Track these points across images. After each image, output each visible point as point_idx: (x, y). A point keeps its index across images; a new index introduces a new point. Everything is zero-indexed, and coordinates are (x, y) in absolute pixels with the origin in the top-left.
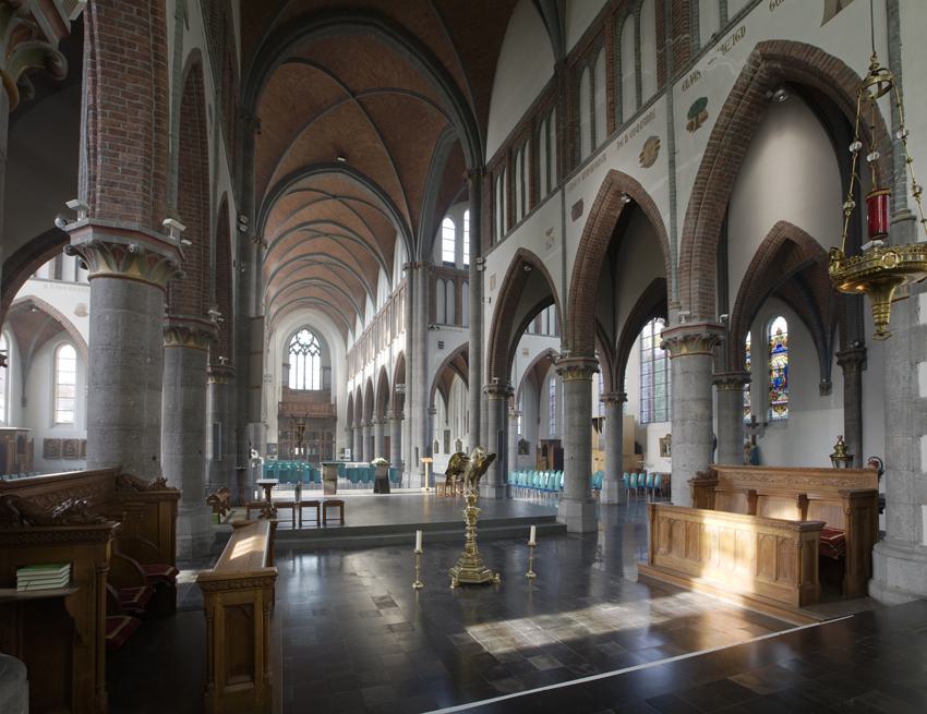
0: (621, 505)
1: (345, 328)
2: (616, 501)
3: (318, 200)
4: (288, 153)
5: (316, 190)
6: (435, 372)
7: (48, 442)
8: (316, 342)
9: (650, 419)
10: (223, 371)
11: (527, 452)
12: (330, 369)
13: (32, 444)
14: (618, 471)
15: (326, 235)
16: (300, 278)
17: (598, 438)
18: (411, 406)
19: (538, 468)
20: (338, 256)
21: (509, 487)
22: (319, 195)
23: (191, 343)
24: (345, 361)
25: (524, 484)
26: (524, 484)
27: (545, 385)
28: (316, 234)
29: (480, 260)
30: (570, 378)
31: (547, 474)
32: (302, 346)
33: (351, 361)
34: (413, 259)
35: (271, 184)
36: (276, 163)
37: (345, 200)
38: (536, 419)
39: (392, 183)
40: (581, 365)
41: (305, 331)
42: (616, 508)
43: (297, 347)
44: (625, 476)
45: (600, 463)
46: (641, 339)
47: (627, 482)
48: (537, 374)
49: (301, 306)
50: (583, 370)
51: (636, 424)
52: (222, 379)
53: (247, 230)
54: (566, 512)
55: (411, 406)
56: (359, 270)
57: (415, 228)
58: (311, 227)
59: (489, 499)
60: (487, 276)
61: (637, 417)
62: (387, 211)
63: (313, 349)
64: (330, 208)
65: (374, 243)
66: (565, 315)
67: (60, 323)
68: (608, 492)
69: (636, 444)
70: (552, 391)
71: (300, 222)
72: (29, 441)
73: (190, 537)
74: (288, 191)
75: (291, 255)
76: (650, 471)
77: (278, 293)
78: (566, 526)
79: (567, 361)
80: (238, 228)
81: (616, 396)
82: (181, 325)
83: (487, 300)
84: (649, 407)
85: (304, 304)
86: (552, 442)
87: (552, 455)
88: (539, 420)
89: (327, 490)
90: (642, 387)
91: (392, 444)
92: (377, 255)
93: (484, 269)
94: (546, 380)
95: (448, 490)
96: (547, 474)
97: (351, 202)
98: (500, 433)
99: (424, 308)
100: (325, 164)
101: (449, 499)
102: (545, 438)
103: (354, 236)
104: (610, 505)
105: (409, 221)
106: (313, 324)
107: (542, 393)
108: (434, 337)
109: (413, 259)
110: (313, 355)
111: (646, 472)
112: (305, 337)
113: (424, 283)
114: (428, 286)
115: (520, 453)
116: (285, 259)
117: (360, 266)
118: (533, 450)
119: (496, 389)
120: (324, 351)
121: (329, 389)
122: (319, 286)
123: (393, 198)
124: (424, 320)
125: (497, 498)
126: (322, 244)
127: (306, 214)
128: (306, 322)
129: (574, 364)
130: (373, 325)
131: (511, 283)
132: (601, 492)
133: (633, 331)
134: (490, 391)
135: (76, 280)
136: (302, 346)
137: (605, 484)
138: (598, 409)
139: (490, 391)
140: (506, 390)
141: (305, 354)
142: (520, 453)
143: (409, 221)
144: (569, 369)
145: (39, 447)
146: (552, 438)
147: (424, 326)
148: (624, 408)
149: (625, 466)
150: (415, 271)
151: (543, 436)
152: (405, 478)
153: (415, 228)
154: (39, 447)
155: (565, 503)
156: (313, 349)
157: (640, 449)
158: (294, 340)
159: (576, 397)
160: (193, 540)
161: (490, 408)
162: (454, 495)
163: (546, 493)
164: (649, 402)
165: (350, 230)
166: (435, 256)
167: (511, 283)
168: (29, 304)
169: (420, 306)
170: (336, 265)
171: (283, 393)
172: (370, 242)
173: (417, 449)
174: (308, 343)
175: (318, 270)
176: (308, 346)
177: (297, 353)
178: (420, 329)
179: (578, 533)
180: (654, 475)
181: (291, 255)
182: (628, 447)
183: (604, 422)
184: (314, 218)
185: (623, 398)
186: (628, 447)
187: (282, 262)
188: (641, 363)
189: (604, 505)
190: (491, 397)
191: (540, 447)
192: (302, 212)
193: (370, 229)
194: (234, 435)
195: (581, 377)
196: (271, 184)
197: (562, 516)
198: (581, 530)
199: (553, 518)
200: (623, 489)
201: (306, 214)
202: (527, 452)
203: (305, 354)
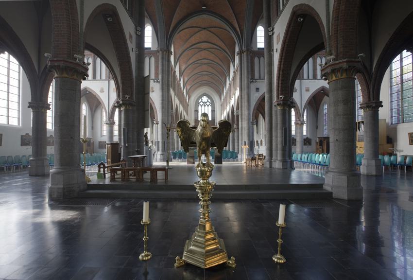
0: (378, 176)
1: (220, 94)
3: (199, 31)
5: (196, 27)
6: (255, 104)
7: (100, 142)
8: (209, 100)
9: (399, 121)
10: (128, 102)
12: (214, 111)
13: (93, 143)
15: (205, 49)
16: (196, 72)
17: (362, 132)
18: (242, 121)
19: (317, 152)
21: (292, 162)
22: (197, 29)
23: (65, 75)
24: (220, 107)
26: (306, 160)
28: (200, 50)
30: (334, 78)
32: (204, 103)
33: (223, 107)
37: (209, 29)
38: (315, 123)
39: (229, 13)
41: (205, 97)
43: (201, 103)
44: (380, 157)
45: (362, 148)
46: (391, 71)
48: (315, 102)
50: (346, 70)
52: (128, 107)
53: (141, 34)
54: (334, 183)
55: (242, 121)
56: (220, 63)
57: (242, 34)
59: (278, 169)
60: (275, 37)
61: (388, 120)
62: (228, 28)
63: (208, 103)
64: (203, 35)
66: (329, 31)
67: (95, 96)
70: (325, 111)
71: (191, 45)
72: (92, 142)
73: (62, 186)
75: (191, 61)
76: (399, 154)
78: (331, 193)
81: (373, 103)
82: (56, 64)
83: (275, 50)
84: (398, 113)
85: (201, 85)
87: (323, 145)
90: (391, 102)
92: (227, 53)
93: (273, 34)
95: (253, 163)
97: (212, 29)
99: (248, 72)
101: (254, 168)
102: (321, 136)
103: (216, 47)
104: (368, 176)
106: (207, 93)
108: (253, 86)
109: (241, 49)
110: (208, 106)
112: (205, 99)
113: (247, 59)
114: (250, 61)
115: (305, 144)
116: (189, 63)
118: (313, 143)
120: (213, 104)
121: (214, 120)
122: (207, 75)
123: (231, 21)
125: (283, 168)
127: (193, 40)
128: (203, 93)
129: (337, 67)
130: (229, 88)
133: (385, 63)
134: (278, 105)
135: (101, 78)
136: (204, 103)
137: (364, 162)
138: (360, 114)
139: (278, 105)
140: (289, 103)
141: (205, 106)
142: (305, 144)
144: (333, 71)
145: (97, 145)
146: (325, 136)
147: (248, 81)
148: (380, 113)
149: (381, 151)
150: (242, 55)
151: (319, 136)
152: (239, 156)
153: (242, 34)
154: (97, 145)
155: (330, 175)
156: (208, 103)
157: (391, 140)
158: (200, 101)
159: (340, 92)
160: (63, 188)
161: (278, 117)
163: (320, 166)
164: (398, 110)
165: (214, 44)
166: (253, 45)
168: (86, 89)
169: (245, 71)
170: (212, 64)
171: (195, 122)
172: (222, 47)
173: (245, 142)
174: (206, 101)
176: (206, 103)
177: (201, 106)
178: (246, 82)
179: (343, 200)
181: (191, 61)
182: (382, 139)
183: (362, 126)
186: (382, 139)
187: (187, 65)
188: (391, 94)
189: (364, 175)
190: (279, 108)
191: (318, 141)
192: (191, 39)
193: (223, 41)
194: (136, 134)
195: (344, 76)
196: (172, 25)
198: (346, 198)
199: (320, 186)
200: (379, 164)
201: (193, 40)
203: (205, 106)
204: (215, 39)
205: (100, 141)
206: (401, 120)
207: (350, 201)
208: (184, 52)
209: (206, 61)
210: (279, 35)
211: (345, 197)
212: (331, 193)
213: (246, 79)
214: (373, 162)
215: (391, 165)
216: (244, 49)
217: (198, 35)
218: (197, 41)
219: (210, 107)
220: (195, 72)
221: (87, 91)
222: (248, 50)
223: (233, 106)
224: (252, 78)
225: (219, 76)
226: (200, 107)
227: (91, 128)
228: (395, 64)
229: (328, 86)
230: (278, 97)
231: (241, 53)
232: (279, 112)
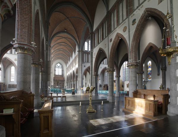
0: (119, 97)
1: (66, 63)
4: (55, 29)
7: (9, 85)
8: (61, 66)
11: (101, 87)
12: (63, 71)
14: (119, 91)
20: (65, 49)
22: (61, 37)
23: (37, 66)
27: (105, 74)
29: (92, 50)
35: (52, 35)
38: (103, 80)
39: (75, 35)
40: (112, 70)
41: (59, 64)
42: (118, 98)
43: (57, 67)
45: (115, 89)
49: (57, 59)
54: (109, 98)
60: (94, 53)
61: (122, 80)
63: (60, 67)
65: (72, 47)
69: (122, 85)
70: (106, 75)
72: (6, 84)
75: (56, 49)
76: (125, 90)
78: (109, 101)
81: (118, 76)
88: (103, 81)
89: (63, 94)
97: (68, 39)
104: (117, 97)
106: (60, 62)
107: (104, 76)
108: (83, 65)
112: (59, 65)
116: (55, 50)
118: (102, 87)
120: (62, 67)
126: (62, 46)
127: (59, 41)
133: (122, 64)
137: (116, 93)
138: (115, 79)
141: (59, 68)
144: (109, 71)
149: (120, 89)
155: (108, 97)
156: (60, 67)
157: (123, 86)
158: (56, 65)
159: (111, 76)
165: (67, 44)
168: (6, 58)
178: (81, 63)
180: (126, 91)
182: (121, 86)
186: (121, 86)
190: (94, 76)
192: (58, 41)
194: (45, 83)
196: (52, 35)
199: (106, 100)
200: (120, 94)
203: (59, 68)
204: (68, 43)
205: (9, 84)
206: (125, 80)
207: (112, 102)
208: (56, 44)
209: (62, 50)
210: (95, 53)
211: (111, 101)
212: (109, 101)
213: (81, 62)
214: (118, 93)
215: (123, 93)
216: (80, 50)
217: (61, 39)
218: (60, 42)
219: (61, 69)
220: (57, 53)
221: (6, 59)
222: (82, 51)
223: (74, 71)
224: (83, 62)
225: (67, 56)
226: (56, 68)
227: (4, 77)
228: (124, 63)
229: (107, 67)
230: (94, 73)
231: (79, 51)
232: (94, 78)
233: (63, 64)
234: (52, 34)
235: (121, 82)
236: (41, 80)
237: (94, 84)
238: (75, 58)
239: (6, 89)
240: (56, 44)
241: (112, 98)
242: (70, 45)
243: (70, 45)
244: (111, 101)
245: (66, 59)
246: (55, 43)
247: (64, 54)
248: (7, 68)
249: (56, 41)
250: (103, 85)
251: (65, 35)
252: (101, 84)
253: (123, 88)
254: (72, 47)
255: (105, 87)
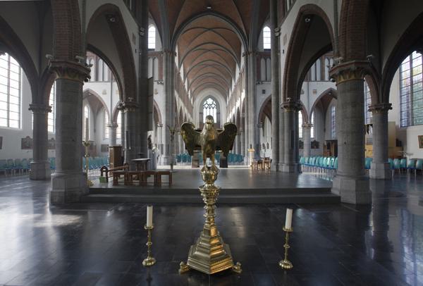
0: (388, 180)
1: (225, 96)
2: (383, 177)
4: (183, 9)
6: (261, 106)
7: (102, 146)
11: (317, 147)
14: (385, 155)
17: (370, 135)
20: (217, 60)
21: (299, 166)
22: (203, 30)
25: (313, 164)
26: (313, 164)
27: (329, 110)
29: (277, 30)
30: (342, 80)
31: (329, 159)
33: (228, 110)
34: (247, 50)
35: (177, 26)
36: (179, 12)
39: (235, 13)
40: (353, 67)
41: (210, 99)
42: (383, 182)
43: (206, 106)
44: (390, 160)
46: (401, 73)
47: (214, 158)
49: (205, 88)
51: (397, 127)
54: (342, 187)
56: (226, 65)
58: (200, 47)
60: (282, 38)
61: (398, 123)
62: (233, 29)
63: (213, 106)
64: (208, 35)
65: (231, 49)
68: (376, 170)
69: (397, 140)
70: (333, 114)
74: (185, 29)
75: (196, 62)
76: (408, 157)
77: (193, 82)
78: (339, 198)
79: (340, 66)
80: (139, 34)
81: (383, 106)
82: (58, 66)
83: (282, 51)
84: (408, 116)
86: (333, 141)
88: (325, 130)
89: (193, 166)
91: (242, 144)
93: (280, 35)
94: (329, 108)
95: (260, 167)
96: (329, 159)
97: (217, 30)
98: (293, 132)
100: (201, 12)
102: (329, 139)
104: (377, 180)
105: (244, 30)
106: (211, 94)
107: (327, 118)
108: (260, 88)
111: (406, 158)
112: (210, 101)
113: (253, 60)
115: (312, 147)
117: (227, 62)
118: (321, 146)
119: (288, 105)
120: (218, 106)
124: (254, 79)
126: (208, 54)
127: (198, 41)
129: (345, 68)
131: (296, 34)
132: (370, 170)
137: (373, 165)
138: (369, 117)
139: (285, 107)
140: (296, 105)
143: (244, 30)
144: (341, 73)
145: (99, 148)
148: (389, 115)
151: (327, 138)
152: (245, 160)
154: (99, 148)
157: (401, 143)
160: (65, 192)
161: (285, 119)
162: (263, 169)
163: (328, 170)
165: (219, 45)
166: (259, 46)
167: (296, 34)
168: (88, 91)
175: (209, 69)
178: (252, 84)
179: (352, 205)
180: (415, 161)
184: (200, 43)
185: (389, 107)
190: (286, 110)
191: (326, 144)
192: (196, 40)
194: (139, 136)
195: (353, 77)
196: (177, 26)
197: (336, 189)
199: (329, 190)
200: (388, 168)
202: (317, 147)
207: (359, 206)
210: (286, 35)
212: (339, 198)
214: (382, 166)
216: (250, 50)
219: (215, 110)
222: (254, 52)
224: (258, 80)
225: (224, 77)
226: (205, 109)
229: (335, 88)
233: (218, 100)
234: (175, 23)
235: (391, 130)
236: (127, 127)
237: (286, 134)
238: (240, 80)
239: (96, 152)
240: (188, 53)
241: (357, 185)
242: (226, 44)
243: (228, 48)
244: (350, 198)
245: (222, 86)
246: (188, 50)
247: (219, 73)
248: (98, 112)
249: (192, 41)
250: (322, 144)
251: (210, 20)
252: (316, 139)
253: (403, 150)
254: (231, 49)
255: (329, 146)
